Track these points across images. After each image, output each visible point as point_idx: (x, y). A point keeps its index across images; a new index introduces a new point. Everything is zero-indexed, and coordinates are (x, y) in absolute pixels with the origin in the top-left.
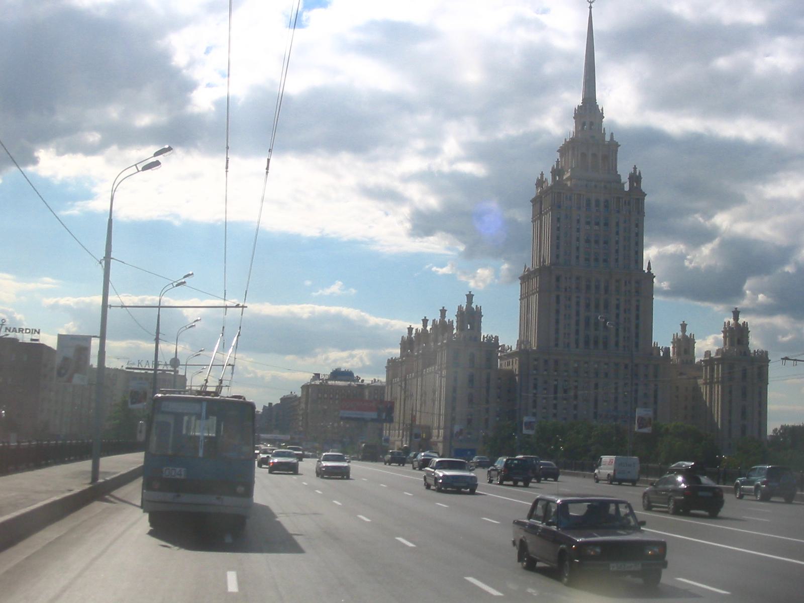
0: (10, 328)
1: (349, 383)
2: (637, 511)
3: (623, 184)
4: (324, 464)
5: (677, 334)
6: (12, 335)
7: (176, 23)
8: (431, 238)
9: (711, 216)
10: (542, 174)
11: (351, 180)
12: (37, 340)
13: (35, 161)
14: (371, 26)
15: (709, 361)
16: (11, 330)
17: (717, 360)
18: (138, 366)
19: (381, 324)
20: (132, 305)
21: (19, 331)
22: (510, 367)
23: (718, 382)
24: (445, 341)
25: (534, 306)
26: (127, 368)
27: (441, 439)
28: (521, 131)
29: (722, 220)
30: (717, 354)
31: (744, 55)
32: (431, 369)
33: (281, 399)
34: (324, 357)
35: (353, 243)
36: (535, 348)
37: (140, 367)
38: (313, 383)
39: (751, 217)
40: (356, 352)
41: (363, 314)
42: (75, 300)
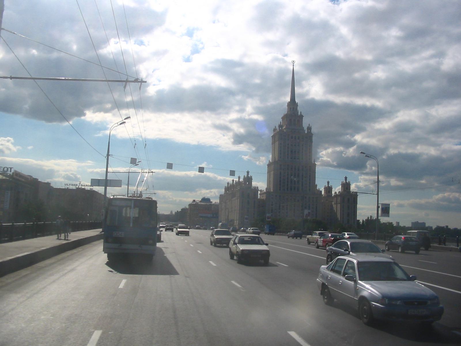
1: (206, 203)
2: (400, 264)
3: (305, 131)
4: (179, 230)
5: (343, 182)
6: (83, 187)
7: (141, 60)
8: (242, 145)
9: (354, 136)
10: (275, 127)
11: (209, 122)
12: (92, 189)
13: (84, 115)
14: (218, 61)
15: (336, 196)
17: (339, 195)
19: (222, 179)
20: (123, 172)
21: (86, 186)
22: (263, 198)
23: (339, 203)
24: (239, 189)
25: (272, 176)
27: (237, 224)
28: (277, 102)
29: (358, 138)
30: (339, 193)
31: (365, 72)
32: (234, 199)
33: (181, 209)
34: (199, 192)
35: (211, 147)
36: (272, 191)
38: (193, 203)
39: (368, 136)
40: (212, 190)
41: (215, 175)
42: (101, 170)
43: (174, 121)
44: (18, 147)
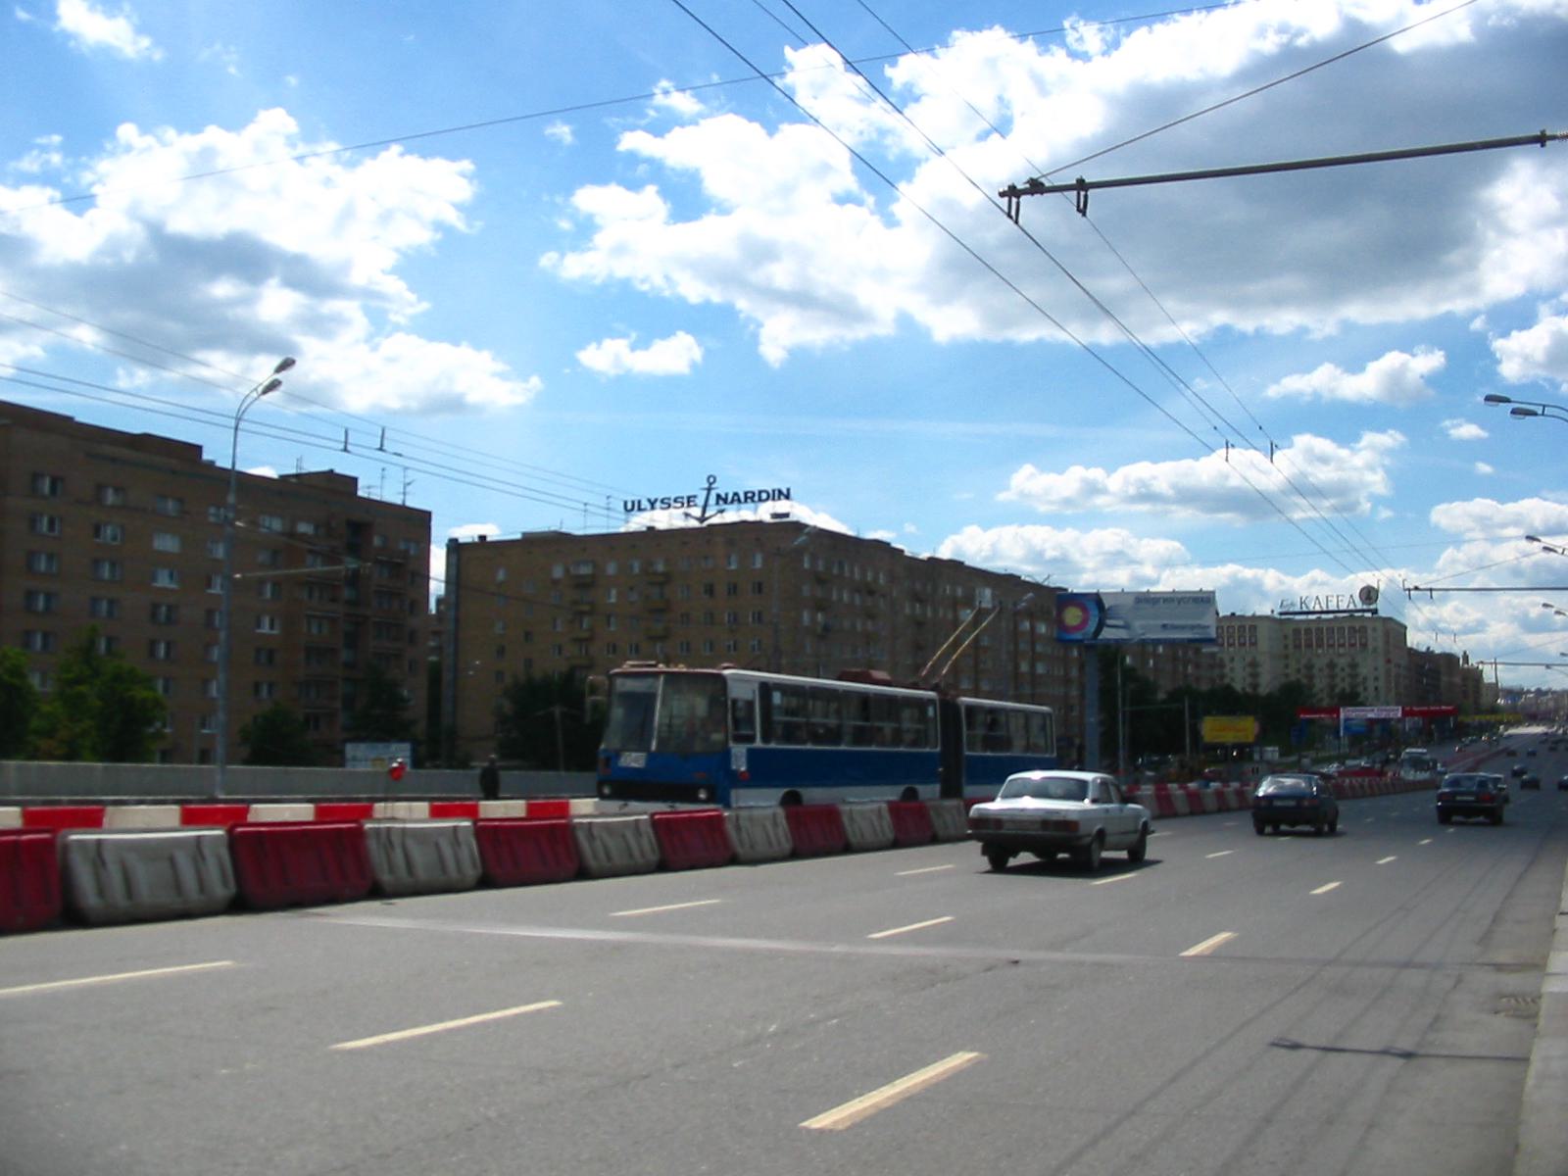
0: (727, 495)
12: (787, 515)
16: (730, 499)
18: (1301, 608)
26: (1281, 614)
37: (1305, 609)
43: (860, 1102)
44: (145, 42)
